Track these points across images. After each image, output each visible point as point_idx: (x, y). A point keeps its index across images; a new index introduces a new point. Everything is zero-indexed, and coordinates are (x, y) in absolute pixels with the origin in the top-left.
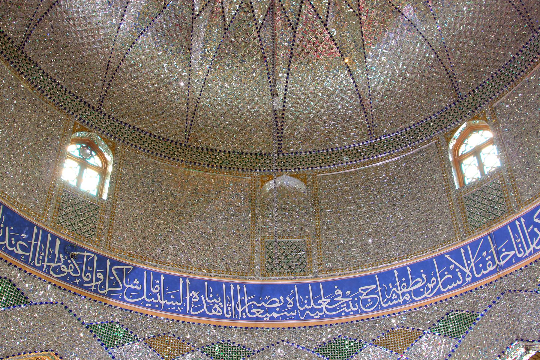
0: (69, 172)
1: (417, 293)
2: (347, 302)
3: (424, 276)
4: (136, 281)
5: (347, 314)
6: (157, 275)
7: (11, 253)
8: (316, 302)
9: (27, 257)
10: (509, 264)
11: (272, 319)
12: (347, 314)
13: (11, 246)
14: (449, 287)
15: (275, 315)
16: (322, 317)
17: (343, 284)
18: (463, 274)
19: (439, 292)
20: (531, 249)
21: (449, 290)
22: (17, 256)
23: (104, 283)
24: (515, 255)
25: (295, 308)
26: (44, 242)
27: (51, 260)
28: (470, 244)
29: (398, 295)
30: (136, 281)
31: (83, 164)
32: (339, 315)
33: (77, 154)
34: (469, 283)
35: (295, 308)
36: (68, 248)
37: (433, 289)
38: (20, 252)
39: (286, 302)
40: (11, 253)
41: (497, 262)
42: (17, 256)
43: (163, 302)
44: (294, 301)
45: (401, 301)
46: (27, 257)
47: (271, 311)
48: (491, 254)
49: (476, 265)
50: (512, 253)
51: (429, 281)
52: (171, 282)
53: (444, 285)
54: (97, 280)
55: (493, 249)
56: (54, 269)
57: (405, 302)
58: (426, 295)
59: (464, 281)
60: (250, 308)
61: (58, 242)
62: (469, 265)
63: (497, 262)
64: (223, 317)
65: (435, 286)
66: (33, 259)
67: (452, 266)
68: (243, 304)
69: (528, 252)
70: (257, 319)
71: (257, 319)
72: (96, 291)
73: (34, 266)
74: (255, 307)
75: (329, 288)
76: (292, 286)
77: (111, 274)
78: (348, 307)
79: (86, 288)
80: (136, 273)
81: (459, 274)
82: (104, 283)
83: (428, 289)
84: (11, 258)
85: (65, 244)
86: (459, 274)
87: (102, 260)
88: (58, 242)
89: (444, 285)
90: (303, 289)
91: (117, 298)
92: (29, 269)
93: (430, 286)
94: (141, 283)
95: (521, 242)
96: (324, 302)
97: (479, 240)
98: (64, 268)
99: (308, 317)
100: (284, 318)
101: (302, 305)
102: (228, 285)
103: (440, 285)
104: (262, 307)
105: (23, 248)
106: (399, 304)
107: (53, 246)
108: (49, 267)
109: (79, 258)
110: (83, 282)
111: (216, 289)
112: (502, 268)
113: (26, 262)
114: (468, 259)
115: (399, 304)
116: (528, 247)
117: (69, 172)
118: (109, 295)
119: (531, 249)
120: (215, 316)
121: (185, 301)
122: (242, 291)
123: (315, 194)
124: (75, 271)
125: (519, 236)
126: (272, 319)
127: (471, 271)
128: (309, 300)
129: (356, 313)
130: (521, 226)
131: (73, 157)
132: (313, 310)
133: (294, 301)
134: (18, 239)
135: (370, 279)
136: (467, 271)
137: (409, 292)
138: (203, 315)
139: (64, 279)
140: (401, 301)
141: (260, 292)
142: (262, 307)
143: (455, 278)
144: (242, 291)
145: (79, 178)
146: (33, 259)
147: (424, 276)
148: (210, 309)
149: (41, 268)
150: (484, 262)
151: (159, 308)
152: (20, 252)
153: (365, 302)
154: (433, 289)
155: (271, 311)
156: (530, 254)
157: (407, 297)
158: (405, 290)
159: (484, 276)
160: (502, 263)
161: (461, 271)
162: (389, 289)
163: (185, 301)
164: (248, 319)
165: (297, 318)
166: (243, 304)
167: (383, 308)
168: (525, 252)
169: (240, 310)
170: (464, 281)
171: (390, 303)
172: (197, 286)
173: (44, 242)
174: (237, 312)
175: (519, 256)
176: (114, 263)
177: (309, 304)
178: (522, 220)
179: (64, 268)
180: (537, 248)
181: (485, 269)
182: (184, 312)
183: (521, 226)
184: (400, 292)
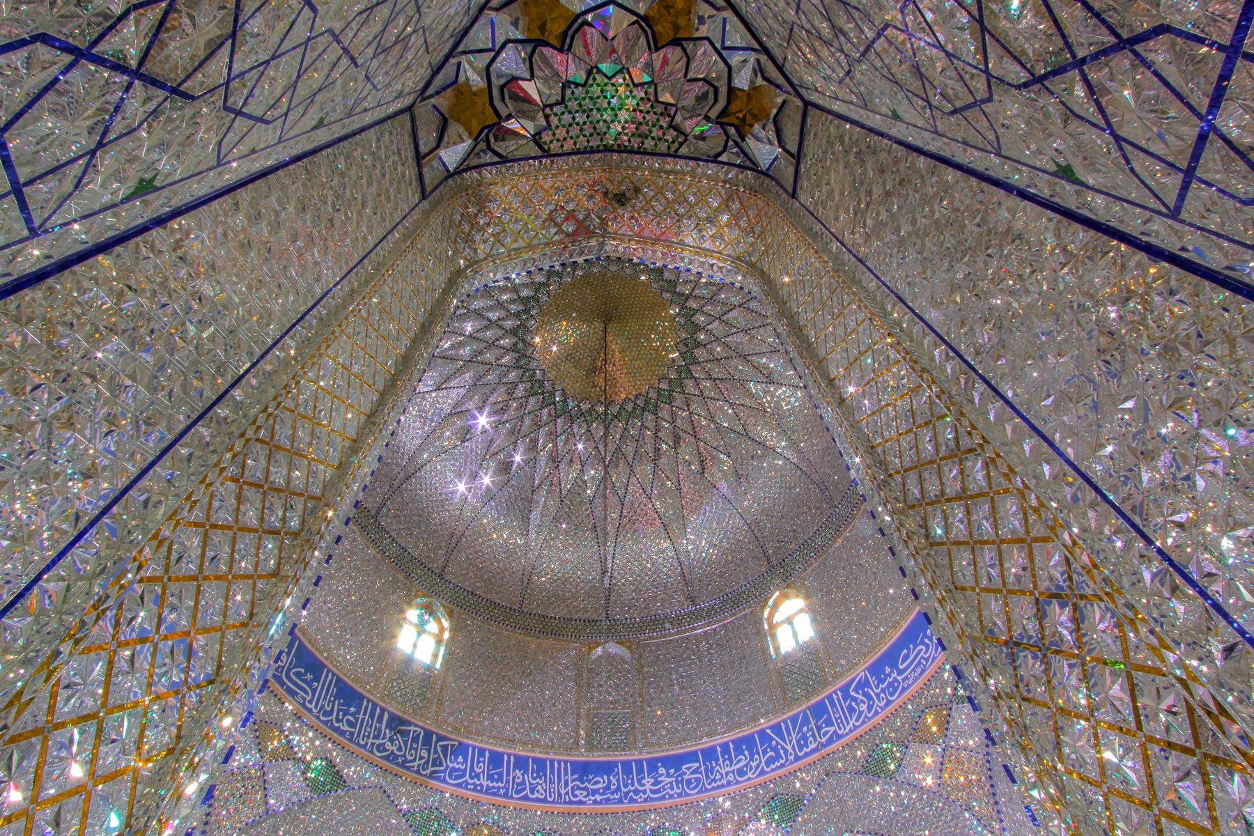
1: (741, 772)
4: (460, 759)
7: (337, 730)
8: (639, 781)
9: (352, 734)
11: (595, 802)
12: (671, 797)
15: (599, 798)
18: (786, 751)
19: (763, 773)
22: (342, 733)
23: (427, 762)
27: (376, 737)
30: (460, 759)
31: (421, 629)
32: (663, 798)
38: (346, 728)
39: (610, 781)
40: (337, 730)
42: (342, 733)
43: (485, 783)
45: (725, 782)
46: (352, 734)
49: (798, 742)
50: (832, 729)
52: (496, 759)
54: (421, 758)
57: (729, 783)
58: (750, 775)
61: (386, 716)
66: (358, 736)
70: (580, 802)
71: (580, 802)
72: (418, 772)
73: (358, 744)
74: (579, 788)
75: (653, 765)
76: (615, 763)
77: (436, 752)
78: (672, 789)
79: (408, 768)
82: (427, 762)
88: (386, 716)
91: (438, 779)
96: (648, 782)
98: (388, 745)
99: (632, 800)
102: (552, 762)
104: (586, 789)
105: (350, 724)
107: (380, 720)
108: (373, 744)
110: (406, 761)
113: (350, 740)
115: (723, 786)
118: (431, 776)
120: (537, 800)
121: (508, 781)
124: (400, 749)
126: (595, 802)
127: (793, 748)
129: (680, 795)
132: (636, 792)
133: (618, 780)
134: (346, 713)
136: (789, 748)
137: (733, 772)
138: (525, 798)
139: (386, 758)
140: (725, 782)
141: (584, 770)
142: (586, 789)
146: (358, 736)
148: (532, 791)
149: (364, 746)
151: (481, 791)
152: (346, 728)
153: (689, 782)
155: (595, 792)
156: (851, 731)
158: (728, 769)
160: (824, 740)
161: (783, 748)
163: (508, 781)
164: (571, 802)
165: (620, 801)
169: (563, 792)
170: (787, 760)
172: (521, 763)
173: (372, 716)
174: (560, 795)
177: (633, 784)
182: (506, 795)
184: (723, 772)
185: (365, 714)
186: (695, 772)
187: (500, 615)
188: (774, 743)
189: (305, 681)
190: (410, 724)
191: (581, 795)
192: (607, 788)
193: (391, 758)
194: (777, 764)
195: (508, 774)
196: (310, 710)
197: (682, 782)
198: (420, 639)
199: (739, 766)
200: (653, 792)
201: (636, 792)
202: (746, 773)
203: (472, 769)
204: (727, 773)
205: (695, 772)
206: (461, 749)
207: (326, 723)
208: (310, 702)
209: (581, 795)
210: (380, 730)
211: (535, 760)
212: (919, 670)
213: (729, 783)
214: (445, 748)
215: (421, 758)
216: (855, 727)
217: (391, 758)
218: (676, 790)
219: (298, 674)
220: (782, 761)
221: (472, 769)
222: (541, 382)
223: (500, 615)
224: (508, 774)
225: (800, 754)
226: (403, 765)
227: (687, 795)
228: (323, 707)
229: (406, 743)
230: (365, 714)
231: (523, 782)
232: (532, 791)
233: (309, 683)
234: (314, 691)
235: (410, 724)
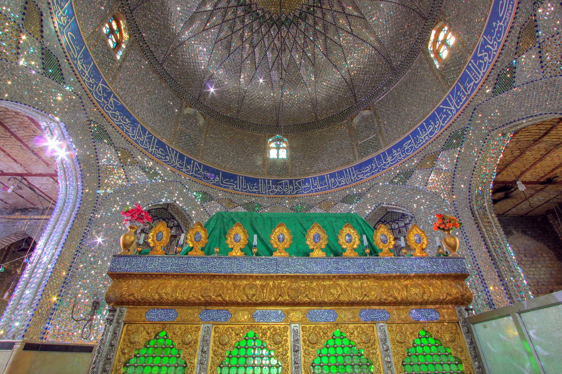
0: (273, 154)
1: (431, 133)
2: (399, 154)
3: (432, 123)
4: (307, 184)
5: (401, 160)
6: (315, 178)
7: (252, 192)
8: (385, 161)
9: (259, 192)
10: (473, 90)
11: (368, 176)
12: (401, 160)
13: (251, 189)
14: (446, 122)
15: (368, 174)
16: (389, 166)
17: (395, 147)
18: (451, 110)
19: (442, 127)
20: (482, 74)
21: (446, 123)
22: (255, 192)
23: (294, 189)
24: (474, 84)
25: (377, 167)
26: (265, 183)
27: (270, 189)
28: (450, 93)
29: (422, 139)
30: (307, 184)
31: (278, 148)
32: (397, 162)
33: (274, 146)
34: (455, 114)
35: (377, 167)
36: (275, 182)
37: (438, 127)
38: (255, 190)
39: (372, 166)
40: (252, 192)
41: (466, 94)
42: (255, 192)
43: (320, 188)
44: (376, 164)
45: (424, 142)
46: (259, 192)
47: (366, 173)
48: (462, 91)
49: (456, 102)
50: (472, 84)
51: (435, 124)
52: (322, 178)
53: (443, 123)
54: (290, 189)
55: (462, 88)
56: (271, 192)
57: (426, 141)
58: (436, 132)
59: (452, 114)
60: (357, 176)
61: (271, 181)
62: (452, 104)
63: (466, 94)
64: (346, 184)
65: (439, 126)
66: (262, 191)
67: (445, 110)
68: (354, 175)
69: (480, 77)
70: (361, 179)
71: (361, 179)
72: (291, 194)
73: (263, 194)
74: (359, 174)
75: (390, 151)
76: (373, 159)
77: (296, 185)
78: (400, 156)
79: (286, 194)
80: (307, 180)
81: (449, 112)
82: (294, 189)
83: (436, 128)
84: (252, 194)
85: (273, 181)
86: (449, 112)
87: (291, 181)
88: (271, 181)
89: (443, 123)
90: (378, 157)
91: (300, 193)
92: (261, 195)
93: (436, 126)
94: (309, 183)
95: (475, 74)
96: (389, 159)
97: (454, 87)
98: (275, 190)
99: (383, 169)
100: (373, 174)
101: (379, 165)
102: (346, 170)
103: (441, 123)
104: (363, 173)
105: (256, 189)
106: (424, 143)
107: (269, 183)
108: (269, 192)
109: (280, 184)
110: (284, 192)
111: (341, 173)
112: (469, 95)
113: (259, 193)
114: (451, 101)
115: (424, 143)
116: (479, 74)
117: (273, 154)
118: (296, 193)
119: (482, 74)
120: (343, 185)
121: (329, 184)
122: (352, 170)
123: (375, 113)
124: (280, 189)
125: (473, 72)
126: (368, 176)
127: (455, 107)
128: (382, 161)
129: (404, 157)
130: (473, 65)
131: (273, 148)
132: (385, 165)
133: (376, 164)
134: (253, 186)
135: (408, 138)
136: (453, 108)
137: (427, 135)
138: (338, 186)
139: (276, 194)
140: (424, 142)
141: (359, 167)
142: (363, 173)
143: (448, 115)
144: (352, 170)
145: (278, 155)
146: (262, 191)
147: (432, 123)
148: (340, 183)
149: (266, 193)
150: (459, 98)
151: (319, 191)
152: (255, 190)
153: (407, 150)
154: (438, 127)
155: (366, 173)
156: (482, 77)
157: (427, 138)
158: (425, 135)
159: (462, 105)
160: (469, 92)
161: (450, 110)
162: (417, 138)
163: (329, 184)
164: (357, 181)
165: (378, 171)
166: (354, 175)
167: (416, 149)
168: (479, 78)
169: (353, 178)
170: (452, 114)
171: (419, 145)
172: (332, 176)
173: (265, 183)
174: (352, 180)
175: (476, 82)
176: (296, 180)
177: (382, 163)
178: (472, 61)
179: (275, 190)
180: (484, 71)
181: (461, 101)
182: (329, 189)
183: (473, 65)
184: (423, 138)
185: (261, 183)
186: (410, 144)
187: (306, 127)
188: (445, 110)
189: (231, 182)
190: (282, 180)
191: (361, 176)
192: (372, 168)
193: (278, 193)
194: (448, 119)
195: (328, 181)
196: (238, 190)
197: (404, 152)
198: (278, 152)
199: (430, 131)
200: (391, 162)
201: (385, 165)
202: (434, 132)
203: (313, 185)
204: (425, 138)
205: (410, 144)
206: (307, 180)
207: (246, 192)
208: (237, 187)
209: (361, 176)
210: (270, 186)
211: (338, 172)
212: (511, 6)
213: (426, 141)
214: (299, 183)
215: (290, 189)
216: (484, 73)
217: (278, 193)
218: (402, 156)
219: (227, 181)
220: (450, 117)
221: (313, 185)
222: (264, 16)
223: (306, 127)
224: (328, 181)
225: (458, 108)
226: (284, 194)
227: (408, 155)
228: (242, 188)
229: (282, 187)
230: (261, 183)
231: (335, 181)
232: (340, 183)
233: (233, 182)
234: (236, 184)
235: (282, 180)
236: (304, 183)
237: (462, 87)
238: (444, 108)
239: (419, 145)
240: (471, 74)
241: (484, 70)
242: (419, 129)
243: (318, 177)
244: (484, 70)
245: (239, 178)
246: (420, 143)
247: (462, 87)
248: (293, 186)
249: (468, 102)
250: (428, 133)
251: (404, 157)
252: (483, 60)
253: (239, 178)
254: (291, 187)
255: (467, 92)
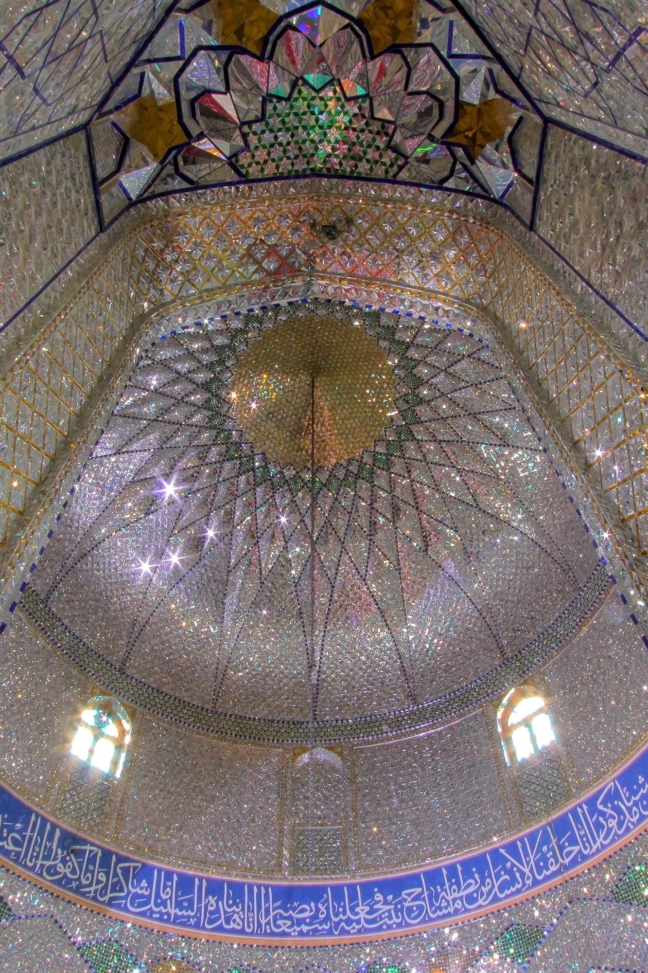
1: (470, 899)
2: (389, 911)
3: (476, 876)
4: (144, 883)
5: (390, 927)
6: (169, 875)
8: (352, 909)
9: (18, 854)
11: (301, 933)
12: (390, 927)
15: (305, 928)
18: (523, 874)
19: (496, 899)
20: (598, 844)
25: (328, 918)
27: (46, 858)
30: (144, 883)
31: (98, 732)
32: (380, 929)
34: (529, 888)
35: (328, 918)
38: (11, 847)
44: (327, 908)
46: (18, 854)
47: (300, 922)
49: (537, 863)
52: (186, 884)
53: (501, 889)
54: (99, 882)
57: (456, 911)
58: (481, 902)
59: (524, 884)
60: (275, 917)
61: (58, 833)
62: (528, 863)
64: (242, 932)
69: (594, 848)
70: (284, 934)
71: (284, 934)
72: (95, 899)
73: (25, 866)
75: (368, 890)
76: (324, 889)
77: (116, 875)
78: (390, 917)
79: (83, 894)
81: (517, 875)
82: (105, 887)
83: (482, 894)
86: (517, 875)
88: (58, 833)
91: (118, 907)
94: (150, 885)
96: (362, 910)
98: (61, 868)
99: (343, 932)
101: (336, 915)
103: (496, 889)
104: (290, 918)
105: (16, 843)
109: (79, 854)
110: (81, 886)
111: (237, 889)
113: (16, 861)
114: (526, 855)
115: (449, 915)
116: (595, 841)
118: (110, 903)
119: (598, 844)
120: (234, 931)
121: (199, 909)
124: (74, 872)
126: (301, 933)
127: (531, 871)
129: (399, 925)
132: (349, 922)
133: (327, 908)
136: (526, 870)
137: (461, 898)
138: (220, 929)
139: (58, 882)
141: (288, 896)
142: (290, 918)
146: (26, 856)
147: (476, 876)
148: (228, 920)
149: (32, 869)
152: (11, 847)
153: (410, 910)
154: (488, 894)
155: (300, 922)
157: (458, 905)
158: (456, 895)
160: (567, 861)
163: (199, 909)
164: (273, 934)
165: (330, 932)
168: (591, 848)
169: (263, 922)
170: (524, 884)
171: (439, 913)
172: (215, 888)
173: (41, 833)
176: (121, 859)
177: (344, 913)
182: (197, 926)
184: (450, 898)
185: (33, 831)
192: (315, 917)
194: (513, 889)
198: (97, 744)
200: (368, 921)
201: (349, 922)
202: (476, 900)
203: (158, 895)
206: (145, 872)
210: (51, 849)
211: (231, 885)
213: (456, 911)
214: (126, 870)
216: (603, 847)
221: (158, 895)
223: (194, 717)
225: (539, 878)
226: (77, 891)
227: (408, 925)
229: (80, 864)
230: (33, 831)
231: (217, 910)
232: (228, 920)
236: (138, 877)
237: (554, 841)
238: (509, 860)
239: (439, 913)
240: (579, 830)
241: (605, 839)
242: (444, 872)
243: (180, 875)
244: (605, 839)
245: (251, 892)
246: (440, 908)
247: (554, 841)
248: (107, 874)
249: (558, 879)
250: (463, 893)
251: (399, 925)
252: (606, 820)
253: (251, 892)
254: (102, 877)
255: (563, 859)
